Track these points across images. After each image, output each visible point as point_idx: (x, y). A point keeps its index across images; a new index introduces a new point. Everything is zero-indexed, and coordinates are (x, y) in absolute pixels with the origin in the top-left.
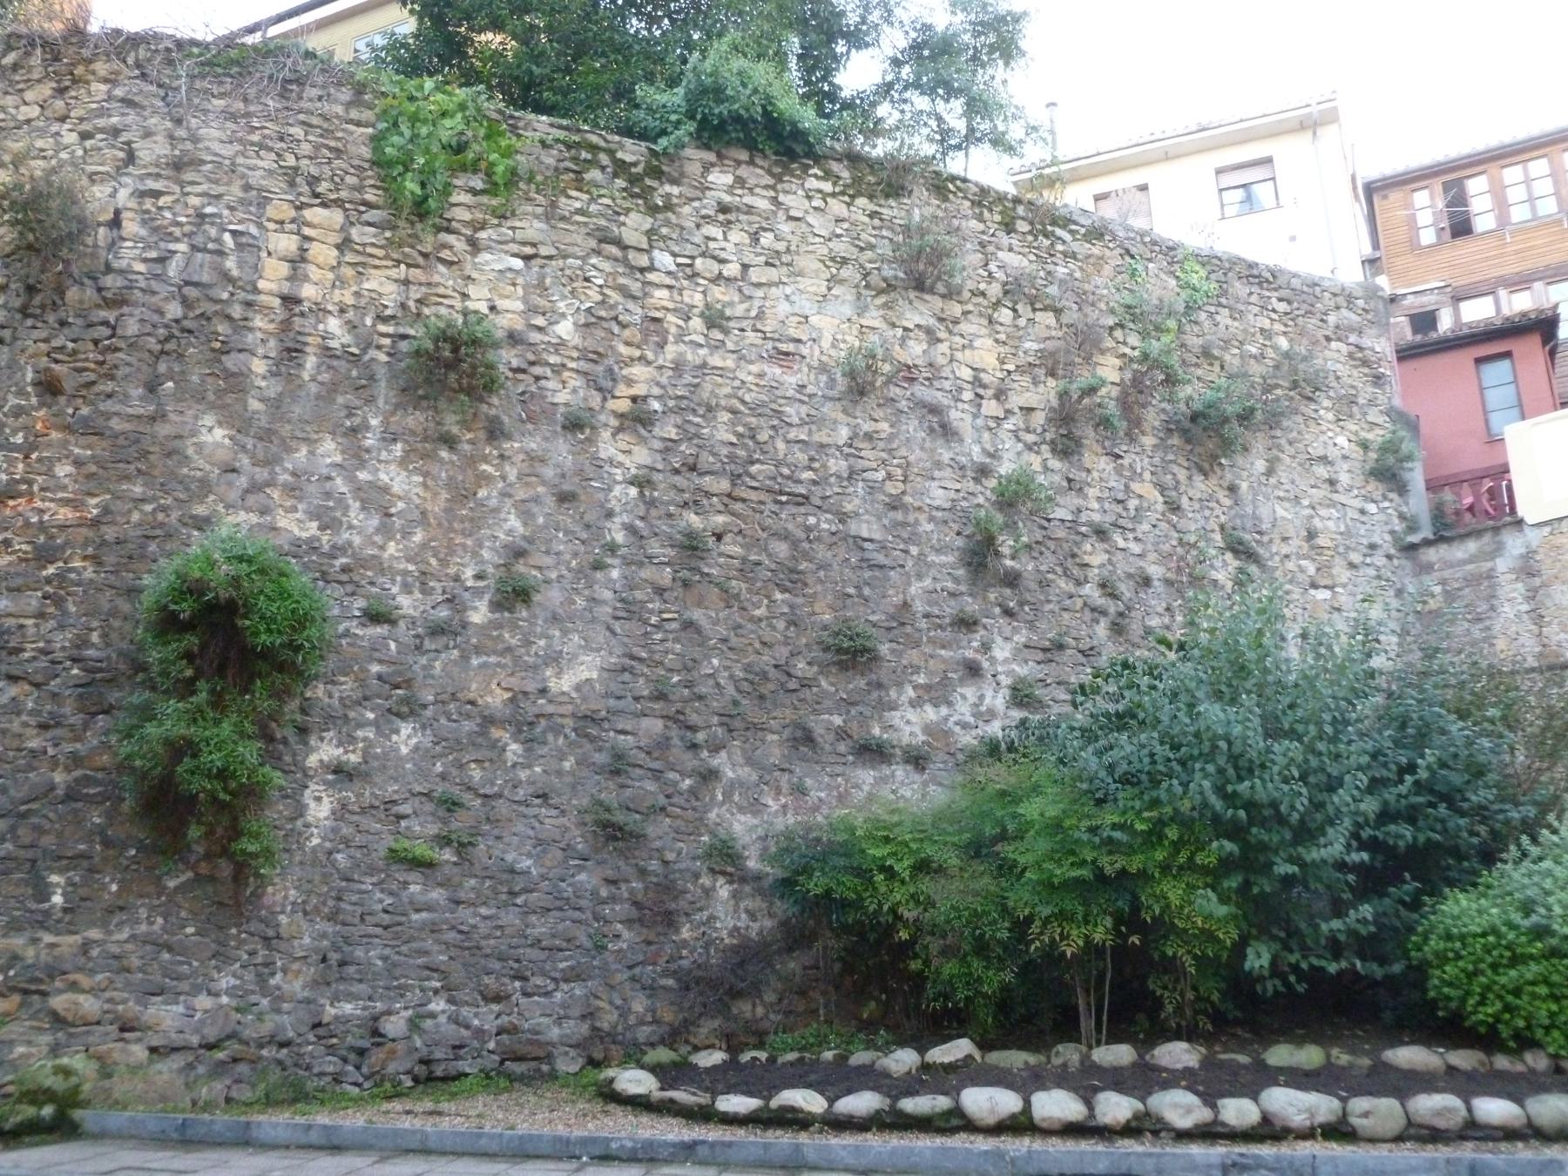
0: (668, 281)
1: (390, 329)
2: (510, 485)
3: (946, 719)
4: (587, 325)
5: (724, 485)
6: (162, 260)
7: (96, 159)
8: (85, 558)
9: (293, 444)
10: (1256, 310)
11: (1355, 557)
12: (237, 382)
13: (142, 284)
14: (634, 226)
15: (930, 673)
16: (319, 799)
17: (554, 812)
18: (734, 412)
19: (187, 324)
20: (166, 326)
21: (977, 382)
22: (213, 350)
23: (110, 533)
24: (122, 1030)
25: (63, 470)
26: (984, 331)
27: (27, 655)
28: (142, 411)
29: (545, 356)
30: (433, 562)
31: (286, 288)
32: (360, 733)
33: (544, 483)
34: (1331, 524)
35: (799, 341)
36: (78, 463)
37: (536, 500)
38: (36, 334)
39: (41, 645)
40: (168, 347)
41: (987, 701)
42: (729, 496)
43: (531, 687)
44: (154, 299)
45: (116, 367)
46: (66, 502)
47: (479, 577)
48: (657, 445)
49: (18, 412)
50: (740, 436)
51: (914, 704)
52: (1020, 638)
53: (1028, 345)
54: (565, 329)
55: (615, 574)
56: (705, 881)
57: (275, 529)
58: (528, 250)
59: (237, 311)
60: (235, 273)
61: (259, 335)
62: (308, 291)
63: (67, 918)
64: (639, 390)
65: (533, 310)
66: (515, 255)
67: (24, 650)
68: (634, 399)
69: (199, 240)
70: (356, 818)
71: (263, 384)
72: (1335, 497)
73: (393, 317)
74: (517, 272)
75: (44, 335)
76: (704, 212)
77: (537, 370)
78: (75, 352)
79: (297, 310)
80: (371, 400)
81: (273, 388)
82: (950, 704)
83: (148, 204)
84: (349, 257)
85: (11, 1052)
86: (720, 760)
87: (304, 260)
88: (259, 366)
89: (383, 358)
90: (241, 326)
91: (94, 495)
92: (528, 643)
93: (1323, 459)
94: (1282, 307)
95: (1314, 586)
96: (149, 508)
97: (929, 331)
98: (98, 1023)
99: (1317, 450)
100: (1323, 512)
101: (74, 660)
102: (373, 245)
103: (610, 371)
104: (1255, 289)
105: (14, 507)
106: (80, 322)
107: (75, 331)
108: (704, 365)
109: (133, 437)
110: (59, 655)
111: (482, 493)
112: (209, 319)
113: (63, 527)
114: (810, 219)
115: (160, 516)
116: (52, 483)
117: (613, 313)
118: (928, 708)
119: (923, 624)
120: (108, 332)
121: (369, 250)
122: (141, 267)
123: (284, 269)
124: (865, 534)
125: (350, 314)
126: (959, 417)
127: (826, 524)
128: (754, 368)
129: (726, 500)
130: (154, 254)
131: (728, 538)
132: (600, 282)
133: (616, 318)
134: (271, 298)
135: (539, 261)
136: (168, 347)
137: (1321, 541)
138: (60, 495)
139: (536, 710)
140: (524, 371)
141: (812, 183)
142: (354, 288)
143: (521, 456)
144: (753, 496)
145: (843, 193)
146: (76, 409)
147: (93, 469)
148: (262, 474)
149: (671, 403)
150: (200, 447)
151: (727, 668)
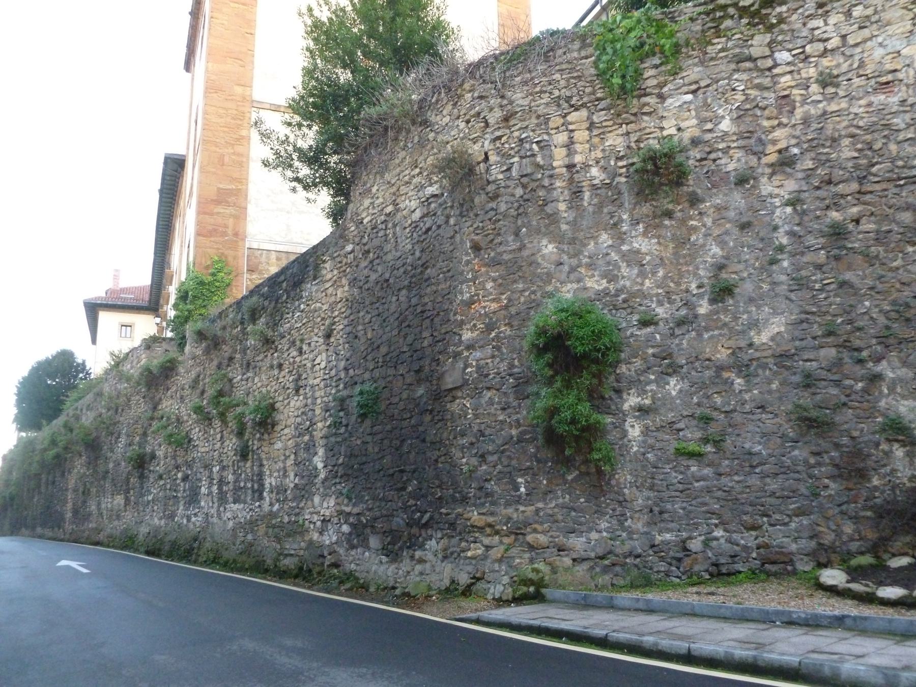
6: (509, 169)
8: (505, 325)
12: (554, 218)
16: (633, 426)
17: (771, 416)
20: (517, 201)
22: (540, 206)
23: (513, 310)
24: (559, 550)
25: (489, 285)
29: (716, 146)
32: (648, 388)
33: (729, 222)
36: (494, 280)
37: (727, 233)
46: (493, 300)
55: (785, 264)
58: (694, 87)
59: (546, 182)
61: (560, 190)
62: (578, 159)
65: (703, 121)
68: (780, 152)
69: (522, 153)
70: (655, 434)
71: (566, 215)
88: (562, 206)
90: (550, 189)
92: (736, 319)
96: (527, 294)
101: (510, 375)
109: (513, 261)
110: (503, 374)
115: (533, 296)
116: (486, 293)
121: (604, 124)
125: (602, 163)
129: (857, 196)
138: (491, 297)
139: (749, 357)
140: (705, 159)
148: (574, 262)
150: (543, 256)
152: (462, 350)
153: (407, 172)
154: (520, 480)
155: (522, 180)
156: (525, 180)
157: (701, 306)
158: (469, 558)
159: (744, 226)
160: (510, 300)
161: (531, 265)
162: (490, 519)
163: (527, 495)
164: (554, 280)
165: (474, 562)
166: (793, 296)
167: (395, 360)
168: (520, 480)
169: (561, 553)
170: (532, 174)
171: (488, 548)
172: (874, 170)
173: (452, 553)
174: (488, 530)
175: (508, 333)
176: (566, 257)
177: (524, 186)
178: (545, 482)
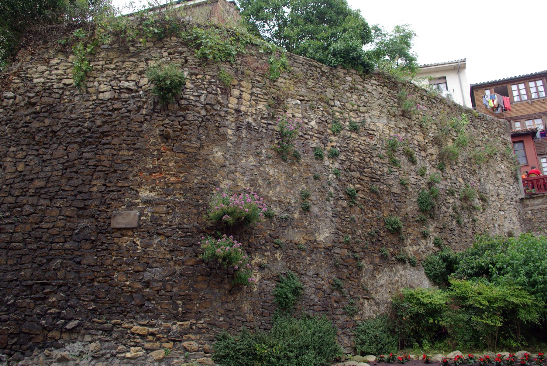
0: (339, 110)
1: (266, 122)
2: (302, 173)
3: (418, 250)
4: (319, 123)
5: (358, 175)
6: (198, 96)
7: (175, 61)
8: (180, 194)
9: (241, 157)
10: (480, 126)
11: (508, 202)
12: (224, 136)
13: (194, 104)
14: (329, 93)
15: (414, 235)
16: (256, 275)
17: (321, 279)
18: (359, 152)
19: (208, 117)
20: (201, 118)
21: (419, 145)
22: (216, 126)
23: (188, 186)
24: (205, 353)
25: (171, 164)
26: (419, 130)
27: (164, 226)
28: (196, 146)
29: (308, 132)
30: (282, 197)
31: (236, 107)
32: (266, 254)
33: (311, 173)
34: (502, 192)
35: (374, 130)
36: (176, 162)
37: (309, 178)
38: (159, 118)
39: (168, 223)
40: (202, 124)
41: (428, 244)
42: (359, 178)
43: (313, 239)
44: (197, 109)
45: (187, 130)
46: (173, 175)
47: (296, 202)
48: (340, 162)
49: (155, 144)
50: (361, 159)
51: (411, 245)
52: (435, 225)
53: (430, 134)
54: (313, 123)
55: (332, 203)
56: (361, 300)
57: (238, 186)
58: (302, 98)
59: (223, 114)
60: (221, 101)
61: (229, 122)
62: (243, 108)
63: (184, 315)
64: (334, 144)
65: (304, 117)
66: (298, 99)
67: (162, 225)
68: (333, 147)
69: (210, 90)
70: (266, 282)
71: (231, 138)
72: (503, 183)
73: (266, 118)
74: (299, 105)
75: (161, 119)
76: (345, 89)
77: (307, 136)
78: (172, 125)
79: (240, 114)
80: (262, 144)
81: (234, 139)
82: (419, 245)
83: (194, 77)
84: (253, 98)
85: (173, 361)
86: (363, 263)
87: (241, 98)
88: (230, 132)
89: (264, 131)
90: (223, 118)
91: (181, 173)
92: (310, 224)
93: (499, 172)
94: (485, 126)
95: (500, 210)
96: (199, 178)
97: (406, 129)
98: (198, 351)
99: (498, 170)
100: (500, 188)
101: (179, 229)
102: (260, 94)
103: (326, 137)
104: (479, 120)
105: (155, 176)
106: (174, 115)
107: (172, 118)
108: (350, 137)
109: (194, 154)
110: (174, 227)
111: (294, 175)
112: (214, 116)
113: (172, 184)
114: (373, 93)
115: (204, 181)
116: (168, 169)
117: (326, 119)
118: (414, 246)
119: (411, 220)
120: (183, 119)
121: (259, 96)
122: (192, 98)
123: (236, 101)
124: (395, 192)
125: (254, 116)
126: (416, 156)
127: (384, 187)
128: (363, 138)
129: (359, 180)
130: (196, 94)
131: (360, 192)
132: (322, 109)
133: (326, 121)
134: (232, 110)
135: (304, 102)
136: (202, 124)
137: (501, 197)
138: (171, 173)
139: (313, 246)
140: (302, 137)
141: (373, 81)
142: (255, 108)
143: (305, 164)
144: (366, 179)
145: (381, 85)
146: (174, 144)
147: (181, 164)
148: (233, 168)
149: (343, 149)
150: (214, 157)
151: (363, 233)
152: (139, 203)
153: (101, 63)
154: (179, 302)
155: (207, 106)
156: (209, 107)
157: (296, 213)
158: (128, 358)
159: (316, 178)
160: (186, 178)
161: (205, 160)
162: (151, 330)
163: (183, 313)
164: (218, 175)
165: (133, 361)
166: (334, 219)
167: (53, 194)
168: (179, 302)
169: (207, 355)
170: (214, 105)
171: (148, 350)
172: (366, 170)
173: (103, 355)
174: (150, 338)
175: (182, 200)
176: (228, 163)
177: (206, 109)
178: (198, 305)
